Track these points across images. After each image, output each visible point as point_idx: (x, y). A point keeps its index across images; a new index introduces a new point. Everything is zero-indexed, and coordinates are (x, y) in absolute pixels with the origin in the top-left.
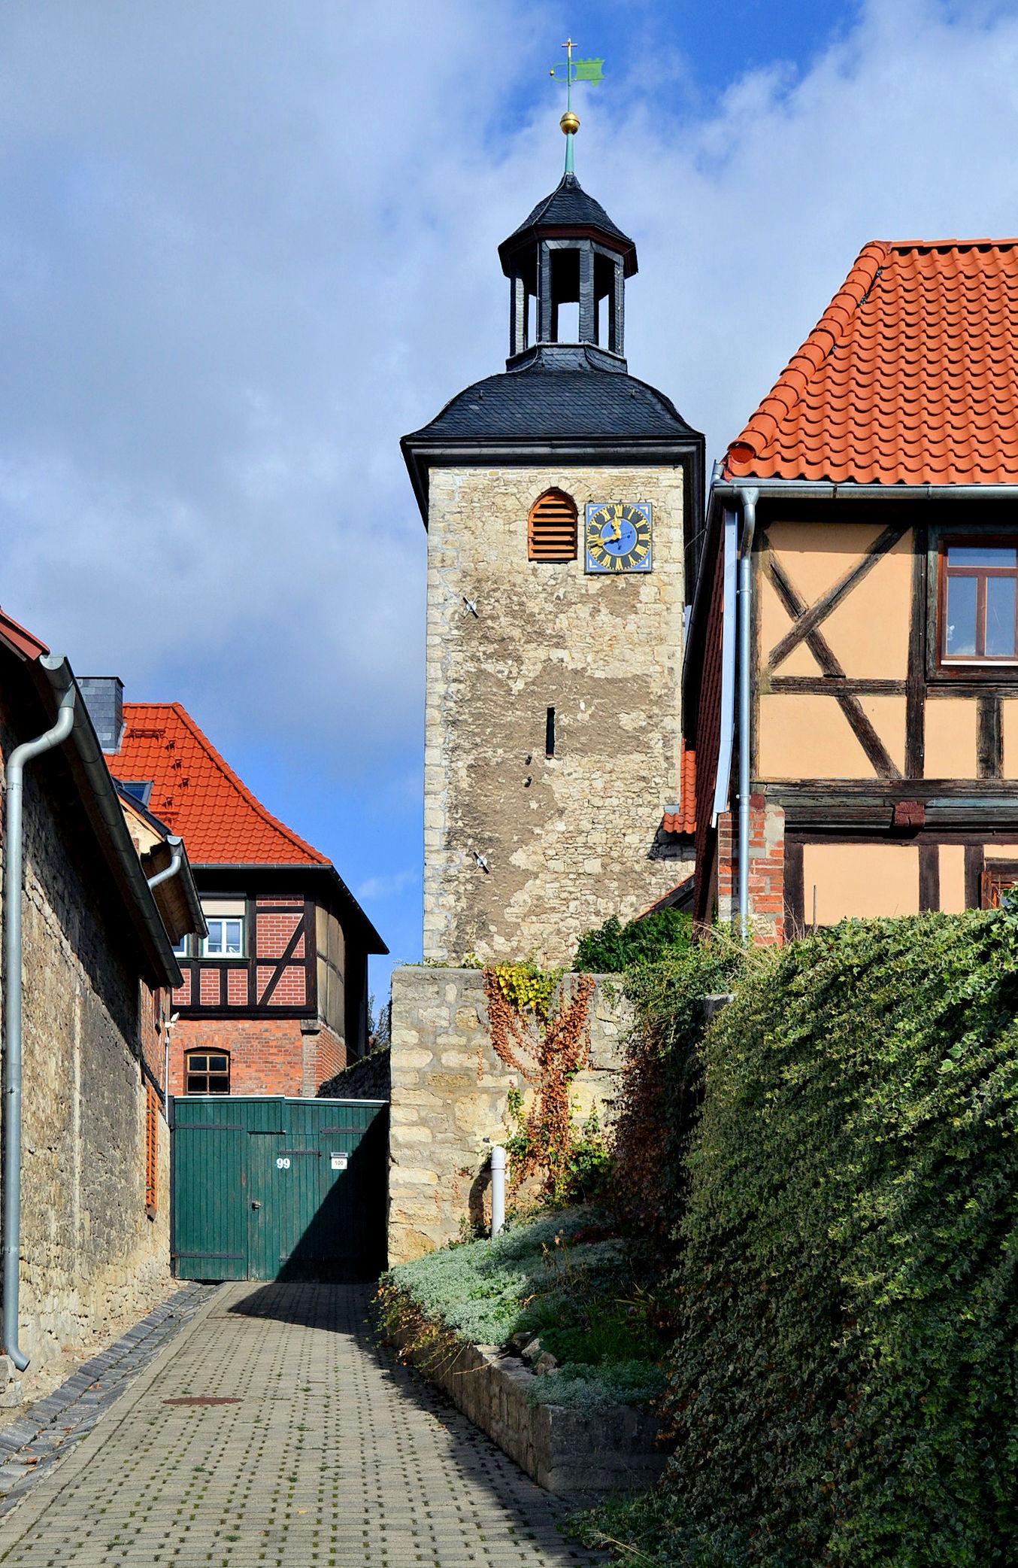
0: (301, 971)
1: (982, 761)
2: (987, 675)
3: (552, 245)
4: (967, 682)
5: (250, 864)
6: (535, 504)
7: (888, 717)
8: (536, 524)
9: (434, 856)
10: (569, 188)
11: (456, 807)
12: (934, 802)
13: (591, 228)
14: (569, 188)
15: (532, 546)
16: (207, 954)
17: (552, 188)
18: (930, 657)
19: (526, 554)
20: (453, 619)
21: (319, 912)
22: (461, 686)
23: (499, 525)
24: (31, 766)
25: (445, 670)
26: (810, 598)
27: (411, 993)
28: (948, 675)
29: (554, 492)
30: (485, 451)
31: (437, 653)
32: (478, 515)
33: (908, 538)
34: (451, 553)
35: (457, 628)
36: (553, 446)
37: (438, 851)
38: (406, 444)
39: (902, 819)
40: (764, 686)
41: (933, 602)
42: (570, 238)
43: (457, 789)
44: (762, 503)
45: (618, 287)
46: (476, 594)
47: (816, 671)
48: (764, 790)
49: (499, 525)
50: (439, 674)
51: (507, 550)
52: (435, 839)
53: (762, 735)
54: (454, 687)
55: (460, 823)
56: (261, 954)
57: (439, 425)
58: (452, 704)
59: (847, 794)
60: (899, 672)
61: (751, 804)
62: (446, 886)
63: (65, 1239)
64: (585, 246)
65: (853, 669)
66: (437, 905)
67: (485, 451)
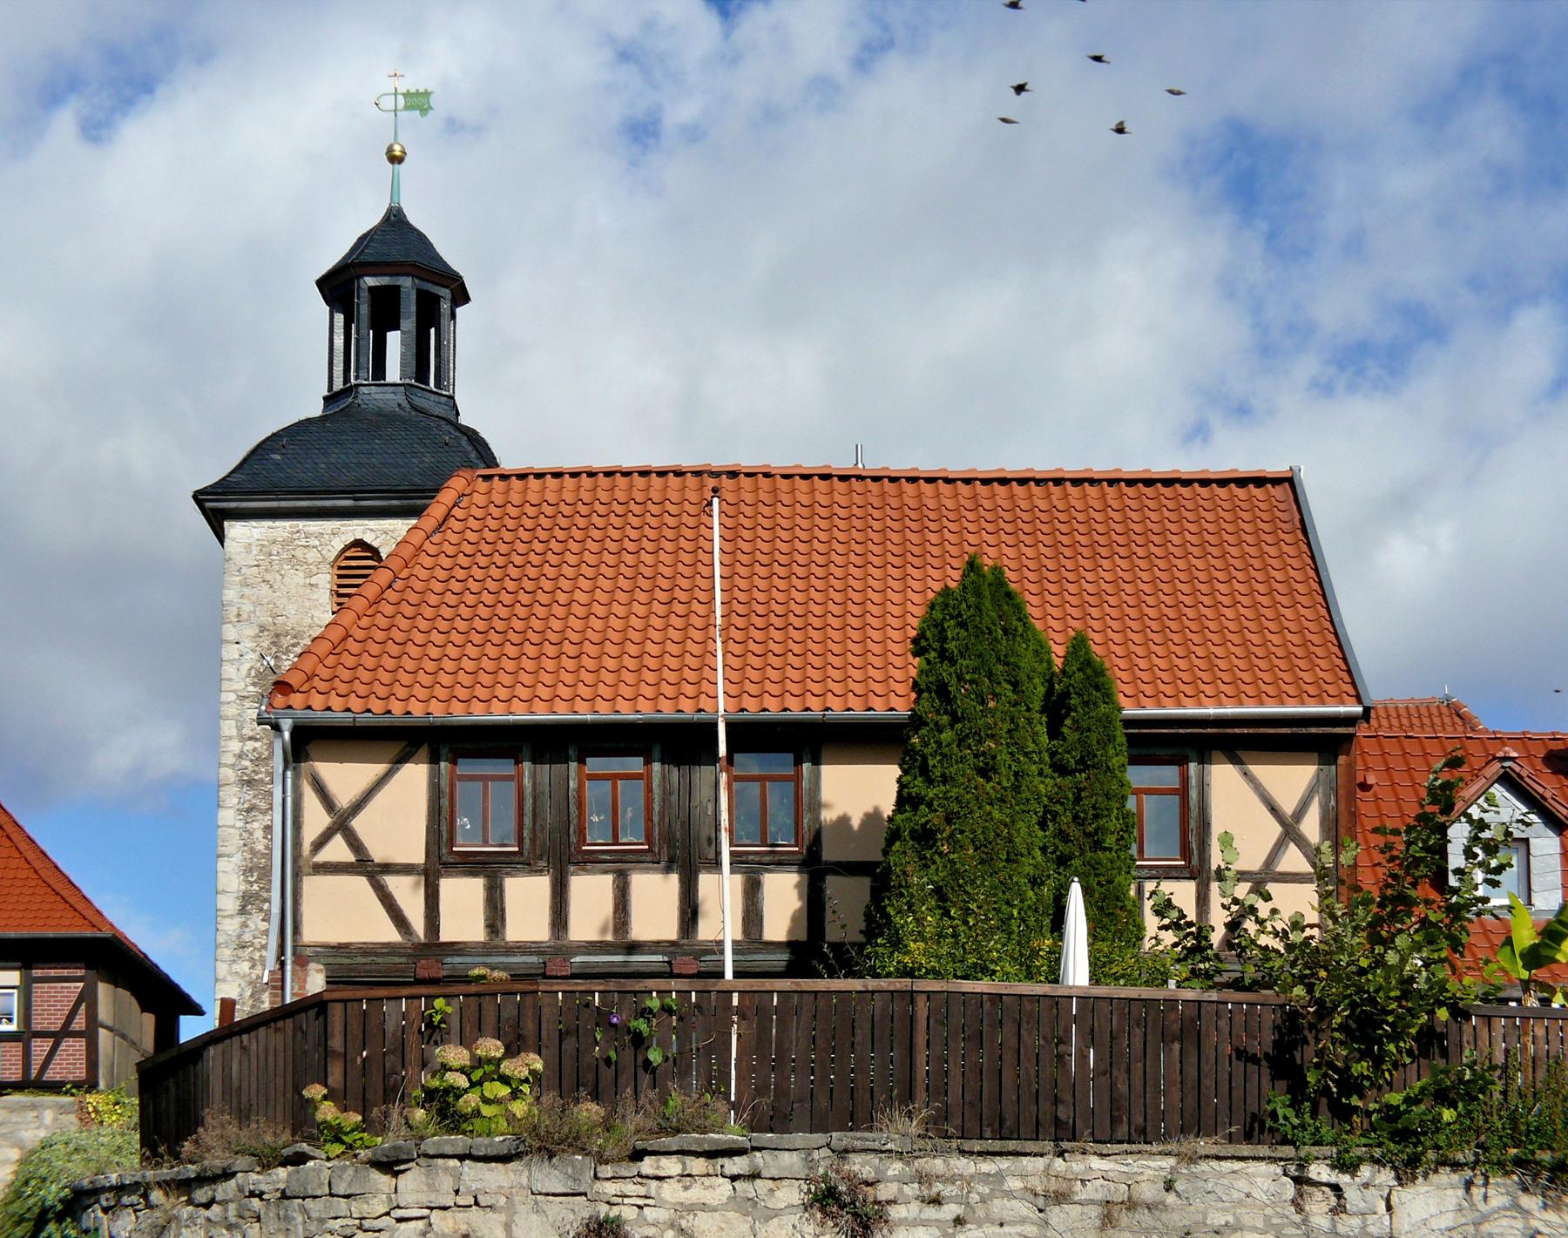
0: (80, 1044)
1: (488, 926)
2: (491, 859)
3: (370, 281)
4: (471, 865)
5: (24, 933)
6: (338, 557)
8: (340, 577)
9: (228, 921)
10: (395, 221)
11: (251, 870)
12: (449, 960)
13: (414, 265)
14: (395, 221)
15: (336, 599)
18: (443, 844)
19: (329, 608)
20: (248, 675)
22: (258, 744)
23: (300, 578)
25: (240, 728)
26: (344, 799)
27: (14, 1118)
28: (458, 859)
29: (359, 543)
30: (283, 504)
32: (276, 567)
33: (424, 751)
34: (247, 607)
35: (254, 684)
36: (355, 499)
37: (230, 916)
38: (199, 497)
39: (423, 974)
40: (306, 869)
41: (445, 802)
42: (390, 275)
43: (253, 852)
45: (444, 321)
46: (274, 649)
48: (308, 952)
49: (300, 578)
50: (234, 732)
51: (307, 604)
52: (229, 903)
53: (306, 908)
54: (250, 745)
55: (255, 887)
56: (36, 1027)
57: (239, 477)
58: (247, 763)
59: (377, 955)
60: (418, 857)
61: (294, 962)
62: (240, 952)
64: (406, 283)
65: (378, 854)
66: (231, 973)
67: (283, 504)
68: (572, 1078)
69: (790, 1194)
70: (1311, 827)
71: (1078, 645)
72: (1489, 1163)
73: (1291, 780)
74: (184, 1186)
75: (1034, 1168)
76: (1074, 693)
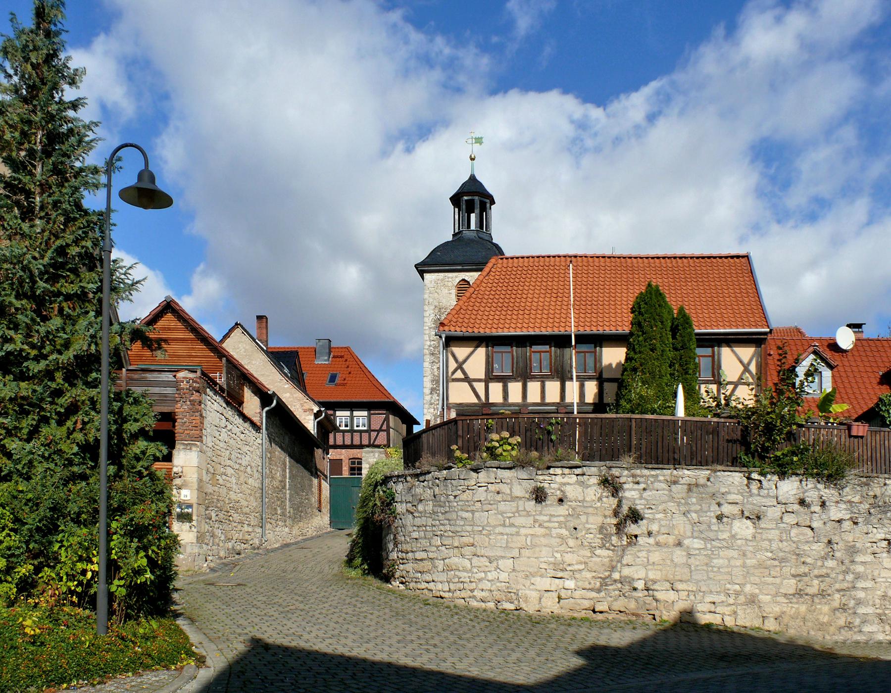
3: (466, 198)
4: (498, 379)
7: (480, 387)
10: (473, 179)
14: (473, 179)
16: (356, 428)
17: (466, 178)
21: (391, 417)
24: (267, 412)
26: (461, 359)
29: (464, 280)
31: (427, 332)
33: (484, 344)
34: (431, 300)
38: (416, 266)
44: (446, 338)
47: (462, 376)
63: (283, 514)
64: (476, 198)
65: (471, 376)
68: (529, 444)
69: (594, 480)
70: (753, 368)
71: (681, 310)
72: (808, 474)
73: (747, 352)
74: (417, 476)
75: (667, 473)
76: (680, 325)
